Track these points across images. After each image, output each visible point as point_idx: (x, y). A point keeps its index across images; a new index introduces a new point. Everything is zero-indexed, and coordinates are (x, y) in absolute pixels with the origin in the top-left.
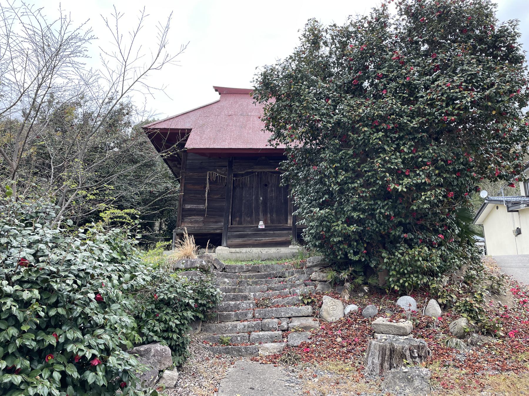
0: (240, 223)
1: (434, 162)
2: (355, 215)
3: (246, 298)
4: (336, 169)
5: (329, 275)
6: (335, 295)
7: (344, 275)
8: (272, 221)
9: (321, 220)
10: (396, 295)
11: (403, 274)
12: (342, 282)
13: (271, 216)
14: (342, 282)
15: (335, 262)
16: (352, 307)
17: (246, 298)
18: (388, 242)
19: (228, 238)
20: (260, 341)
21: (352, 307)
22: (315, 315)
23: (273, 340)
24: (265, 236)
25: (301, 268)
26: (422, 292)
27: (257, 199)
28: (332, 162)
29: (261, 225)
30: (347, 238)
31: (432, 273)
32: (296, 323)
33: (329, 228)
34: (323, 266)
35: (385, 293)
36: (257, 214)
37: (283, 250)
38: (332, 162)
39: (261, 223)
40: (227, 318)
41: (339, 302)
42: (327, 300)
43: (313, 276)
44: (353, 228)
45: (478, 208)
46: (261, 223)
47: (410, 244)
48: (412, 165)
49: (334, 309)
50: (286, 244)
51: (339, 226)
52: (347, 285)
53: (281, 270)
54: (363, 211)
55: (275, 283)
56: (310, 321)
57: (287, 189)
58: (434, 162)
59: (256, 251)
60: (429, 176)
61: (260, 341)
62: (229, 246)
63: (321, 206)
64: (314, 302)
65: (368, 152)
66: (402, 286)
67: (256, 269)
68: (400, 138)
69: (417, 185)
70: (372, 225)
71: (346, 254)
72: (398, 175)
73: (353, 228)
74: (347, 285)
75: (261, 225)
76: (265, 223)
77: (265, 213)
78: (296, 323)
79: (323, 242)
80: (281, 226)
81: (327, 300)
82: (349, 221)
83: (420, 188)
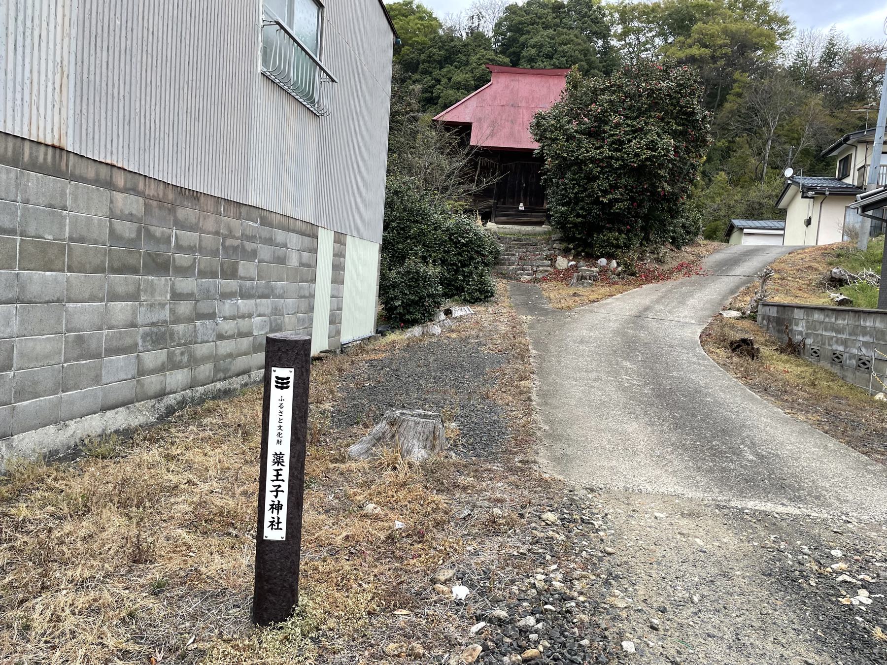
0: (504, 203)
1: (626, 187)
2: (581, 212)
3: (514, 255)
4: (574, 185)
5: (563, 246)
6: (565, 257)
7: (571, 246)
8: (531, 204)
9: (562, 213)
10: (598, 258)
11: (603, 247)
12: (571, 250)
13: (530, 199)
14: (571, 250)
15: (566, 239)
16: (573, 263)
17: (514, 255)
18: (600, 230)
19: (496, 216)
20: (522, 274)
21: (573, 263)
22: (551, 266)
23: (528, 274)
24: (524, 216)
25: (547, 241)
26: (610, 257)
27: (520, 184)
28: (573, 180)
29: (521, 207)
30: (576, 225)
31: (618, 247)
32: (541, 268)
33: (566, 218)
34: (561, 240)
35: (592, 257)
36: (519, 196)
37: (538, 229)
38: (573, 180)
39: (521, 204)
40: (504, 264)
41: (566, 260)
42: (559, 258)
43: (555, 246)
44: (579, 220)
45: (126, 374)
46: (521, 204)
47: (610, 230)
48: (614, 187)
49: (562, 263)
50: (540, 224)
51: (571, 218)
52: (573, 251)
53: (534, 241)
54: (586, 211)
55: (531, 248)
56: (549, 268)
57: (544, 188)
58: (626, 187)
59: (517, 228)
60: (622, 195)
61: (522, 274)
62: (497, 223)
63: (563, 205)
64: (552, 259)
65: (591, 178)
66: (601, 253)
67: (519, 240)
68: (609, 172)
69: (615, 199)
70: (590, 218)
71: (574, 234)
72: (605, 192)
73: (579, 220)
74: (573, 251)
75: (521, 207)
76: (524, 205)
77: (525, 198)
78: (541, 268)
79: (562, 225)
80: (536, 212)
81: (559, 258)
82: (578, 216)
83: (617, 200)
